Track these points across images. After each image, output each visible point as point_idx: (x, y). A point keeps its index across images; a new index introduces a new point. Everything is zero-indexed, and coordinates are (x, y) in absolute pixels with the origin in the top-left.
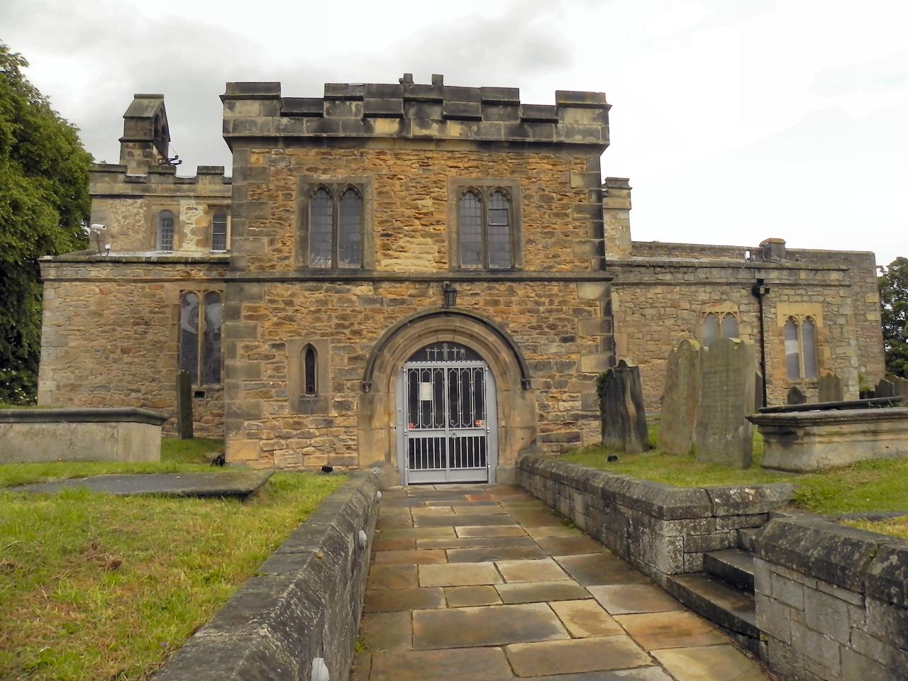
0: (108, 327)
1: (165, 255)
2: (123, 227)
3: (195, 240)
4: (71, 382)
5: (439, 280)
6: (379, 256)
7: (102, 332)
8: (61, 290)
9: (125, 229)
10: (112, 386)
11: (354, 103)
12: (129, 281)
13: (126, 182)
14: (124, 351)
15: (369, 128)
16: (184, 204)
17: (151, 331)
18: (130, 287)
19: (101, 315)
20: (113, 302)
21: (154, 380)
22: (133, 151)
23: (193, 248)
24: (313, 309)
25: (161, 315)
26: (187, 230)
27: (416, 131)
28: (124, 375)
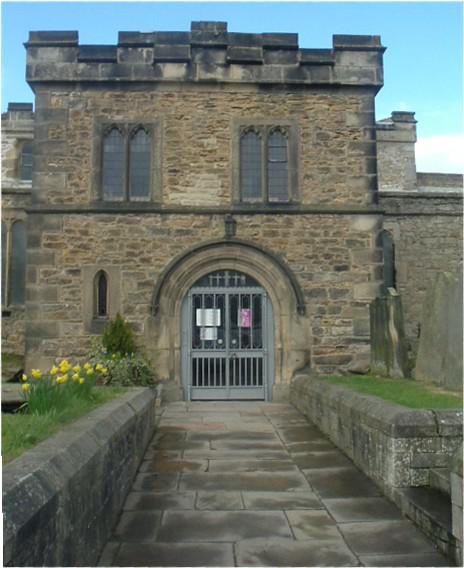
15: (159, 73)
27: (201, 74)
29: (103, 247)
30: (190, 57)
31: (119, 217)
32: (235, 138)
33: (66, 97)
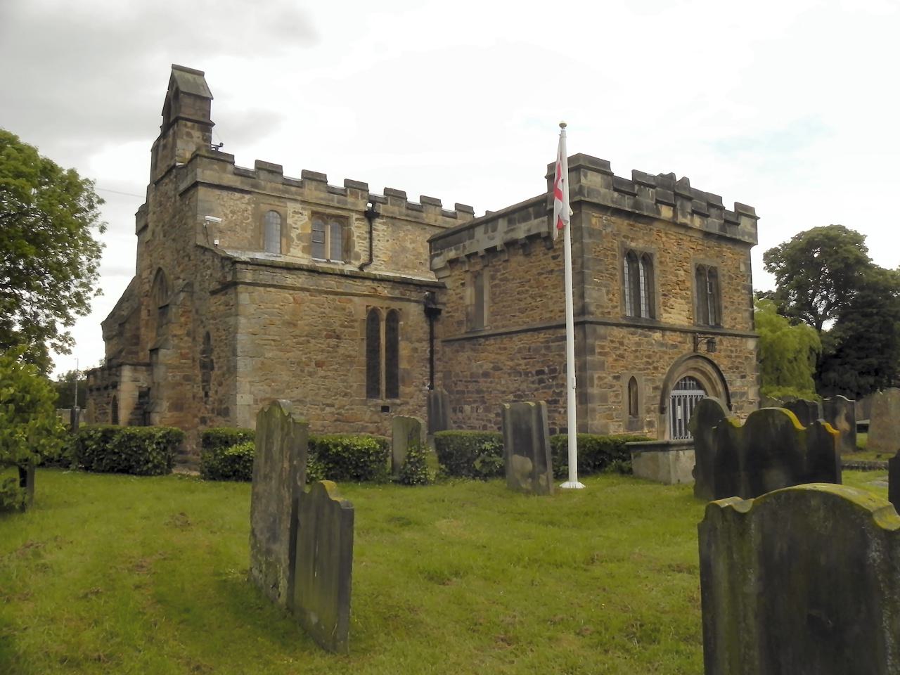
0: (303, 339)
1: (271, 259)
2: (230, 222)
3: (301, 247)
4: (268, 396)
5: (694, 332)
6: (662, 311)
7: (297, 343)
8: (255, 295)
9: (233, 225)
10: (308, 399)
11: (651, 190)
12: (321, 292)
13: (235, 174)
14: (319, 364)
15: (659, 212)
16: (291, 207)
17: (342, 344)
18: (322, 298)
19: (295, 325)
20: (306, 313)
21: (346, 394)
22: (192, 132)
23: (300, 254)
24: (634, 349)
25: (350, 329)
26: (294, 235)
27: (681, 220)
28: (319, 389)
29: (632, 356)
30: (673, 202)
31: (640, 331)
32: (693, 272)
33: (600, 219)
